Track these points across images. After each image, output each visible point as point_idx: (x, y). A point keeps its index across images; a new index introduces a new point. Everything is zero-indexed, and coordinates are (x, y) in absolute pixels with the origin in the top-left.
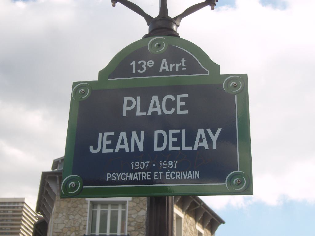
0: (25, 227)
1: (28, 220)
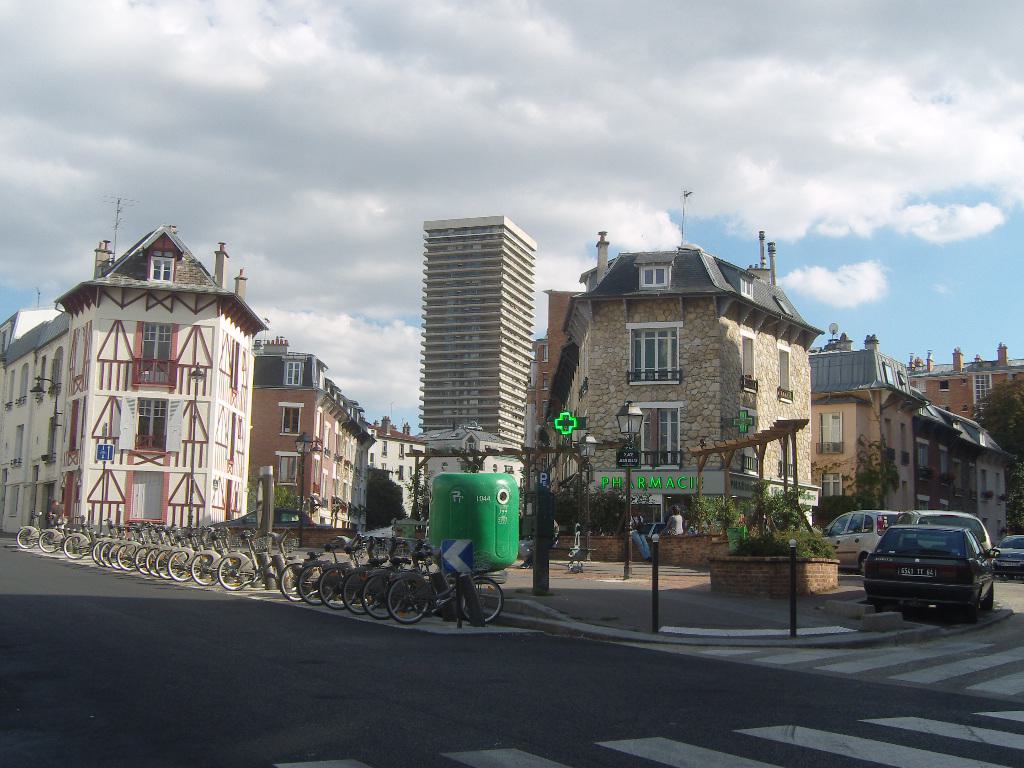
0: (509, 275)
1: (515, 262)
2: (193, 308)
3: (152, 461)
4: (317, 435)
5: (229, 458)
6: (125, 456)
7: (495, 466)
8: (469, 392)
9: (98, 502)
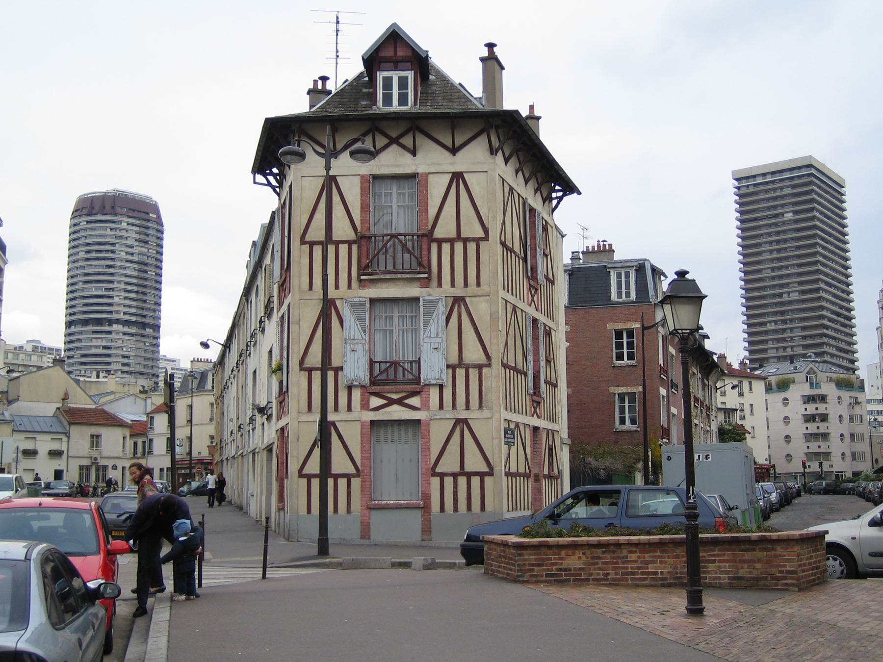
2: (450, 145)
3: (400, 402)
4: (661, 362)
5: (531, 391)
6: (356, 394)
7: (839, 398)
8: (791, 329)
9: (315, 476)
